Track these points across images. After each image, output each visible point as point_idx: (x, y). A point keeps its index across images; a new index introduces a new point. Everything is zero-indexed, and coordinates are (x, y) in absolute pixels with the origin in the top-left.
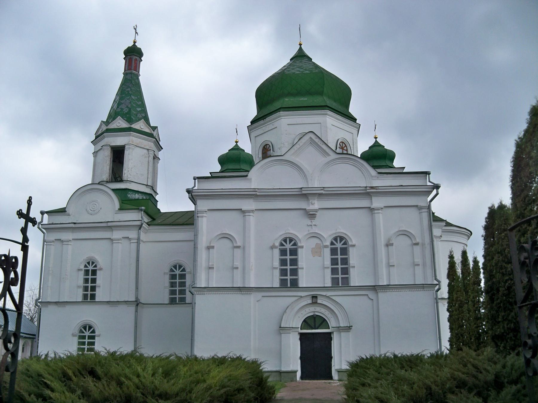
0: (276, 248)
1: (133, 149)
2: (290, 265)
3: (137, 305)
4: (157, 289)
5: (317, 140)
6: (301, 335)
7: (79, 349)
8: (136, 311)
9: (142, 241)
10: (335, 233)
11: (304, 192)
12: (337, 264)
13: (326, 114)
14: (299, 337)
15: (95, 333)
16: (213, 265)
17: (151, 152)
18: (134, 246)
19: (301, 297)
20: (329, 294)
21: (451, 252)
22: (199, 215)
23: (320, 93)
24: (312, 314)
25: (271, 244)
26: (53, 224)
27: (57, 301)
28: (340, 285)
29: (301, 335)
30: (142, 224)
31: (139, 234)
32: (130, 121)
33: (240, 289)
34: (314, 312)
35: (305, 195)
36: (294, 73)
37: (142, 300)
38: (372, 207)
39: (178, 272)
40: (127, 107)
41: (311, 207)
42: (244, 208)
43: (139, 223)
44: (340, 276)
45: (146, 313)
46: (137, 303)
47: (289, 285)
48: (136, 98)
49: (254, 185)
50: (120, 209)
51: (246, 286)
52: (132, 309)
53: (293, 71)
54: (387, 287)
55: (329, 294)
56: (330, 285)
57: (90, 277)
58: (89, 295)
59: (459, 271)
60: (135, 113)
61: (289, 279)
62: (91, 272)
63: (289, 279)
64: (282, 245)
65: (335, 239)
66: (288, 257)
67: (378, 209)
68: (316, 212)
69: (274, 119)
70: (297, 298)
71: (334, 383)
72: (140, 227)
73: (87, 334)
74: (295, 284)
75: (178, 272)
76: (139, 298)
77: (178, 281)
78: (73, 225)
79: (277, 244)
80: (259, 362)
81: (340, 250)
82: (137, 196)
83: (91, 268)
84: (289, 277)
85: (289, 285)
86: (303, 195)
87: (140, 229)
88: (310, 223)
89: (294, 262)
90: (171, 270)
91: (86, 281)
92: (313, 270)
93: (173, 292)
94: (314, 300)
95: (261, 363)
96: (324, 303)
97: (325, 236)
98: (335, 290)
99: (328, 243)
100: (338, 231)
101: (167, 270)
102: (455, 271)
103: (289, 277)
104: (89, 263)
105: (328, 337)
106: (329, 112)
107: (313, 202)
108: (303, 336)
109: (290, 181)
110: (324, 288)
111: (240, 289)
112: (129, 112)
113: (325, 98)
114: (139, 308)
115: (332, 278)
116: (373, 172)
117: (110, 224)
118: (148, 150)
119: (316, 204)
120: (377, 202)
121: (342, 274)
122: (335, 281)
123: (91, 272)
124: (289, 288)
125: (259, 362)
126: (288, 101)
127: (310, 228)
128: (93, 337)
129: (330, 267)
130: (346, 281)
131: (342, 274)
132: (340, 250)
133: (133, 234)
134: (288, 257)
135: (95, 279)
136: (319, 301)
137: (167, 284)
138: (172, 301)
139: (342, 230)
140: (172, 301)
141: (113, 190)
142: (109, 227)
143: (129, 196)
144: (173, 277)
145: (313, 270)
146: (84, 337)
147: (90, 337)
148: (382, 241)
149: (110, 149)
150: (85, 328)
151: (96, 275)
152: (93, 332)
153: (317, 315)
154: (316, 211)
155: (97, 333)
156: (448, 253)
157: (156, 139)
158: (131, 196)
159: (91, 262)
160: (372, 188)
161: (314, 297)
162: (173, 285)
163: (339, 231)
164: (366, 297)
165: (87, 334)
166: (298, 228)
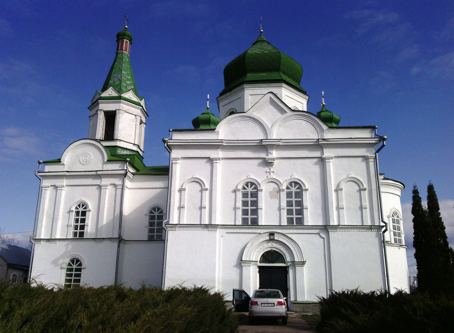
0: (239, 190)
1: (123, 114)
2: (251, 206)
3: (120, 242)
4: (138, 229)
5: (276, 100)
6: (260, 267)
7: (67, 280)
8: (119, 246)
9: (127, 187)
10: (291, 179)
11: (263, 143)
12: (292, 206)
13: (281, 87)
14: (258, 270)
15: (81, 266)
16: (184, 205)
17: (138, 118)
18: (119, 191)
19: (260, 234)
20: (284, 231)
21: (415, 187)
22: (173, 162)
23: (277, 70)
24: (270, 249)
25: (234, 188)
26: (49, 172)
27: (49, 238)
28: (295, 224)
29: (260, 267)
30: (127, 173)
31: (123, 182)
32: (120, 91)
33: (206, 226)
34: (272, 247)
35: (264, 146)
36: (256, 53)
37: (125, 237)
38: (323, 156)
39: (156, 214)
40: (119, 80)
41: (270, 156)
42: (212, 156)
43: (123, 172)
44: (295, 216)
45: (128, 249)
46: (120, 240)
47: (250, 224)
48: (126, 73)
49: (221, 136)
50: (109, 161)
51: (212, 223)
52: (115, 245)
53: (255, 51)
54: (335, 227)
55: (284, 231)
56: (286, 224)
57: (80, 217)
58: (78, 233)
59: (425, 204)
60: (125, 85)
61: (250, 220)
62: (81, 213)
63: (250, 220)
64: (244, 188)
65: (291, 184)
66: (249, 199)
67: (329, 159)
68: (274, 160)
69: (238, 91)
70: (256, 235)
71: (292, 314)
72: (125, 175)
73: (75, 267)
74: (255, 223)
75: (156, 214)
76: (122, 235)
77: (156, 221)
78: (67, 174)
79: (240, 187)
80: (222, 294)
81: (295, 194)
82: (125, 152)
83: (81, 209)
84: (249, 217)
85: (250, 224)
86: (262, 146)
87: (125, 177)
88: (268, 170)
89: (255, 203)
90: (151, 212)
91: (77, 221)
92: (270, 212)
93: (151, 231)
94: (272, 237)
95: (223, 296)
96: (281, 239)
97: (282, 182)
98: (290, 229)
99: (284, 187)
100: (293, 177)
101: (147, 213)
102: (420, 206)
103: (249, 217)
104: (83, 206)
105: (285, 270)
106: (284, 85)
107: (272, 152)
108: (262, 270)
109: (253, 134)
110: (280, 226)
111: (206, 226)
112: (120, 85)
113: (281, 74)
114: (122, 245)
115: (288, 218)
116: (325, 127)
117: (99, 173)
118: (136, 115)
119: (275, 154)
120: (328, 153)
121: (296, 215)
122: (290, 221)
123: (81, 213)
124: (249, 225)
125: (222, 294)
126: (250, 76)
127: (268, 174)
128: (80, 270)
129: (286, 208)
130: (300, 222)
131: (296, 215)
132: (295, 194)
133: (118, 181)
134: (249, 199)
135: (85, 219)
136: (276, 238)
137: (147, 223)
138: (151, 239)
139: (297, 176)
140: (151, 239)
141: (106, 147)
142: (98, 175)
143: (119, 152)
144: (152, 218)
145: (270, 212)
146: (71, 270)
147: (77, 270)
148: (332, 186)
149: (103, 113)
150: (83, 206)
151: (85, 216)
152: (80, 265)
153: (274, 251)
154: (274, 159)
155: (83, 267)
156: (412, 189)
157: (142, 107)
158: (120, 152)
159: (84, 205)
160: (324, 140)
161: (272, 234)
162: (151, 224)
163: (294, 177)
164: (317, 236)
165: (74, 267)
166: (258, 174)
